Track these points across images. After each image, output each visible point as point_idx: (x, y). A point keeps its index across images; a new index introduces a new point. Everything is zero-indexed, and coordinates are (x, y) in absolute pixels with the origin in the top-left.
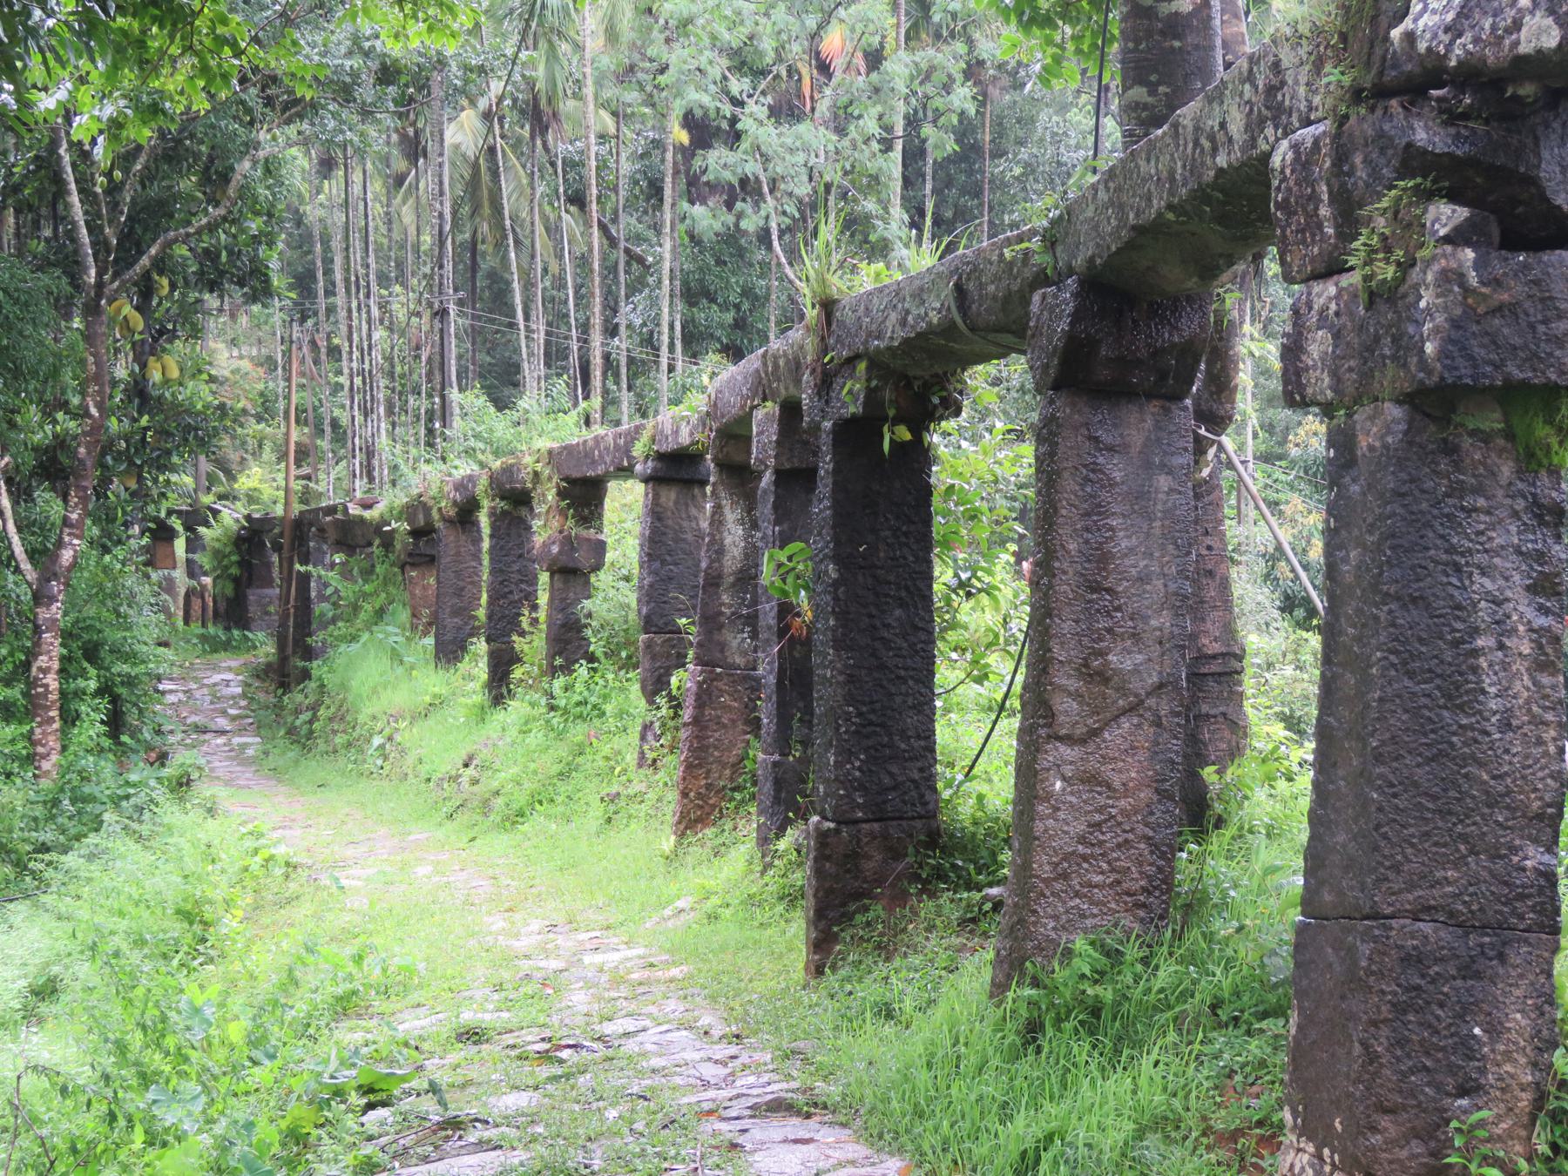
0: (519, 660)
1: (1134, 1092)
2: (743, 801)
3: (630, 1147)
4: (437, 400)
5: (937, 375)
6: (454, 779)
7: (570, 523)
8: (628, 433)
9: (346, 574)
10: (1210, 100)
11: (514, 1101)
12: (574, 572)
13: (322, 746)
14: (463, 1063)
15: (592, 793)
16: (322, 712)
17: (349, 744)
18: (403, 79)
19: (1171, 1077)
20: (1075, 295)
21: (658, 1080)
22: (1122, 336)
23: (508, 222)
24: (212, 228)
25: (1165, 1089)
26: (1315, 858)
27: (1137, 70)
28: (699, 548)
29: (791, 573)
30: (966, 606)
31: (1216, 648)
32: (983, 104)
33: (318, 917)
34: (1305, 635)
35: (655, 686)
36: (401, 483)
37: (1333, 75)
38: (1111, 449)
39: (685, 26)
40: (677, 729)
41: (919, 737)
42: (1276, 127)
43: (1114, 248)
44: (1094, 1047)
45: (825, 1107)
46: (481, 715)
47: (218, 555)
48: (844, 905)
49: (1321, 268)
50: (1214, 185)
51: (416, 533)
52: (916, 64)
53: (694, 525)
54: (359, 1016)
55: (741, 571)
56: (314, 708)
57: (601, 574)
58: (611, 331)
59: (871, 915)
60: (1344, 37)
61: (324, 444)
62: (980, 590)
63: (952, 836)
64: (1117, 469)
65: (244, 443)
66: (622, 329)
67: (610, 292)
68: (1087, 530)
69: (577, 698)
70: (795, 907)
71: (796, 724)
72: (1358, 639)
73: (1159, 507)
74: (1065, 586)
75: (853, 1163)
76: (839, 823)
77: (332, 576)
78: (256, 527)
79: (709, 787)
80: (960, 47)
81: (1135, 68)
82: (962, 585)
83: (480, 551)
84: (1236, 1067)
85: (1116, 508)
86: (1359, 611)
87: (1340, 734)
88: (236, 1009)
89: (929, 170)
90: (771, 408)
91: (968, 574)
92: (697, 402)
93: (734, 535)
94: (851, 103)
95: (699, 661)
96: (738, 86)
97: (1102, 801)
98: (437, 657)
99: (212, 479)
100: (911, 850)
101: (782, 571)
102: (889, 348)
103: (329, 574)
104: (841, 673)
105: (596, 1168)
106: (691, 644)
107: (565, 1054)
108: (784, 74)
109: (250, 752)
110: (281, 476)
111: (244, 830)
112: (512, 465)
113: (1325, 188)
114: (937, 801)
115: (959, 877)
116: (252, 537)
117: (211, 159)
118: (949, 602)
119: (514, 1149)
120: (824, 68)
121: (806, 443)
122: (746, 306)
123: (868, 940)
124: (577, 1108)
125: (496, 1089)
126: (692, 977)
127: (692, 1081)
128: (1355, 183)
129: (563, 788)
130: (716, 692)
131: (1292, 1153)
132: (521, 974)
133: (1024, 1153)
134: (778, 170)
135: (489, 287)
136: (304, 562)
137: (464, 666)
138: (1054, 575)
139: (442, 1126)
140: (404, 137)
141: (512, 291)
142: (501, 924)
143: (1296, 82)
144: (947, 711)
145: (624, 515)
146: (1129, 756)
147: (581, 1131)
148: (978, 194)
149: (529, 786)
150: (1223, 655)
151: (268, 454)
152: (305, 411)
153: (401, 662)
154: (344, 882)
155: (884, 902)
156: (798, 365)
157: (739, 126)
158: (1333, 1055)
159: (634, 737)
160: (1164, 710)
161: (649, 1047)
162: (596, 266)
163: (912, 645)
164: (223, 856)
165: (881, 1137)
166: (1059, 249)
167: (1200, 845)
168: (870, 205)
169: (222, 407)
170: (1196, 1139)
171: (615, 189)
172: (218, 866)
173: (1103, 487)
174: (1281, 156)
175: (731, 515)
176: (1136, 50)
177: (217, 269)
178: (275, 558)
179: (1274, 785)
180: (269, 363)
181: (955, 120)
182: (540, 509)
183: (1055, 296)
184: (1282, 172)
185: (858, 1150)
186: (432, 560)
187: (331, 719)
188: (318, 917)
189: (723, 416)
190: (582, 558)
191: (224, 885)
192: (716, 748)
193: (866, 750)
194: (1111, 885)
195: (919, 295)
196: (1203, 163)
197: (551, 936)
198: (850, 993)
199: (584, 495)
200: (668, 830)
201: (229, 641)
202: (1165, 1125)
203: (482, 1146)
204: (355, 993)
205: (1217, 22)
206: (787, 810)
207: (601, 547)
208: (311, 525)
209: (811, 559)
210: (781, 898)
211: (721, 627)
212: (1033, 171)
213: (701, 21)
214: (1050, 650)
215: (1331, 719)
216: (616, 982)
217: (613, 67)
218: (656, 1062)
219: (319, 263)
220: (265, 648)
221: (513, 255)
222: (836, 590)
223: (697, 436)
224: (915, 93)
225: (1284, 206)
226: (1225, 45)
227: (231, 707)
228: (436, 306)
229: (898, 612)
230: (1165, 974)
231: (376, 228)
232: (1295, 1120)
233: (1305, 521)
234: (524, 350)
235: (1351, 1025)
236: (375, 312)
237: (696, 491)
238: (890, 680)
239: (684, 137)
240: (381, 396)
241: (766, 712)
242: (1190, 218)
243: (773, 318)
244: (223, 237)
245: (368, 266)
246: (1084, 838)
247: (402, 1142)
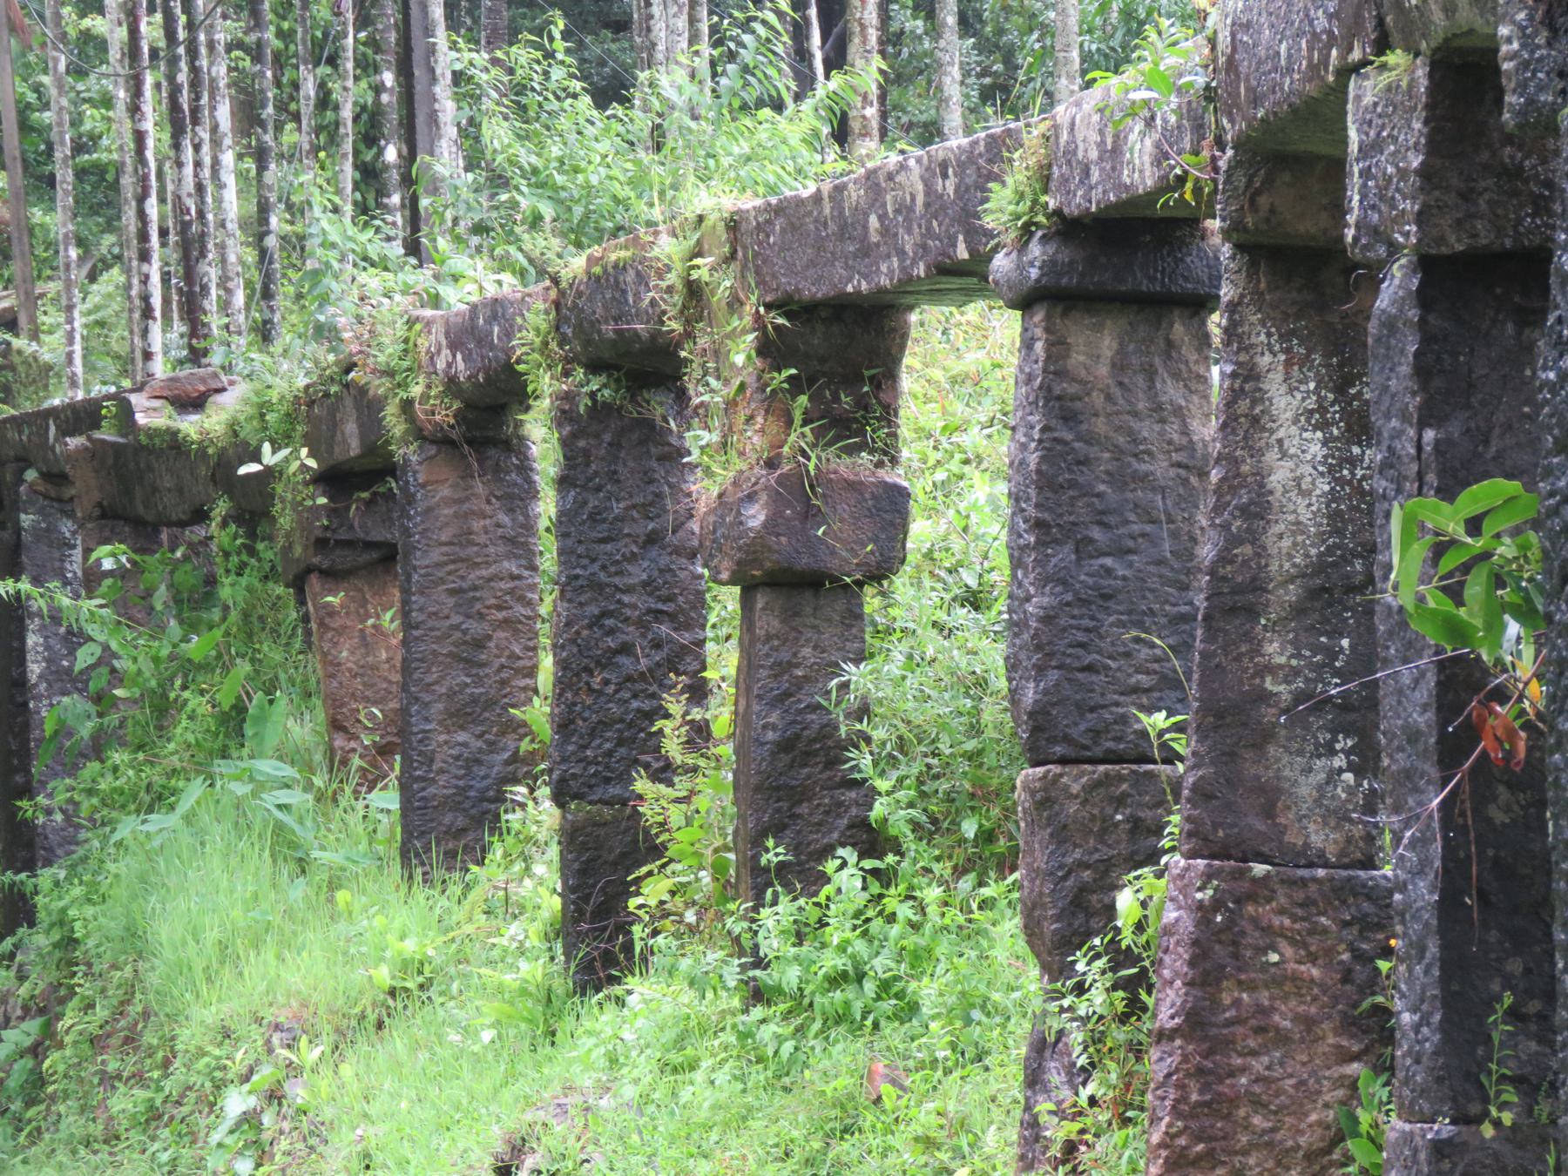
8: (968, 159)
9: (133, 607)
12: (814, 583)
13: (72, 1123)
16: (70, 1018)
17: (153, 1116)
28: (1189, 501)
35: (1069, 922)
55: (1320, 567)
56: (47, 1008)
61: (54, 220)
69: (831, 962)
83: (529, 527)
93: (1297, 461)
95: (1200, 842)
101: (1449, 562)
121: (1514, 173)
130: (1253, 937)
137: (490, 874)
153: (303, 866)
159: (1007, 1077)
175: (1287, 401)
182: (708, 393)
186: (386, 559)
187: (97, 1042)
189: (1256, 101)
190: (838, 540)
192: (1258, 1104)
199: (839, 351)
207: (891, 508)
209: (1536, 524)
211: (1266, 736)
223: (1180, 163)
241: (1408, 993)
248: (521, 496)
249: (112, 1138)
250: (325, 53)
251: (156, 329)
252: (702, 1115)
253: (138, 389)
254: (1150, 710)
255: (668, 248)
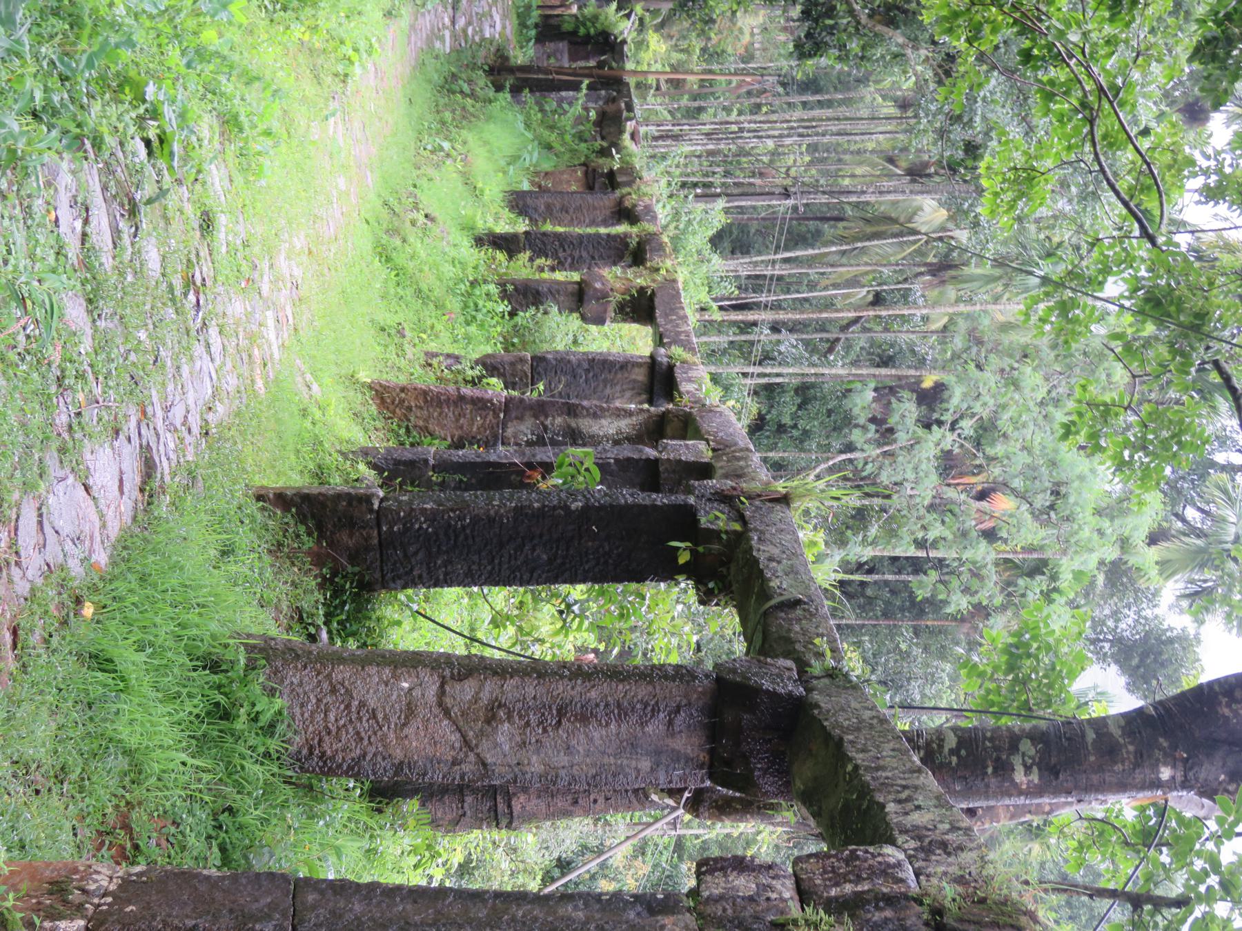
0: (511, 257)
1: (161, 747)
2: (398, 435)
3: (116, 351)
4: (718, 190)
5: (731, 586)
6: (416, 207)
7: (619, 297)
8: (689, 342)
9: (579, 120)
10: (938, 798)
11: (153, 258)
12: (579, 299)
13: (442, 101)
14: (184, 217)
15: (405, 316)
16: (469, 101)
17: (443, 123)
18: (970, 163)
19: (173, 776)
20: (790, 694)
21: (170, 370)
22: (756, 734)
23: (859, 245)
24: (851, 12)
25: (164, 771)
26: (342, 888)
27: (968, 740)
28: (600, 399)
29: (576, 474)
30: (554, 611)
31: (517, 808)
32: (955, 619)
33: (304, 100)
34: (539, 877)
35: (491, 366)
36: (653, 162)
37: (950, 891)
38: (671, 723)
39: (1013, 384)
40: (456, 383)
41: (446, 574)
42: (915, 849)
43: (826, 723)
44: (198, 716)
45: (149, 504)
46: (467, 227)
47: (595, 18)
48: (313, 517)
49: (805, 886)
50: (873, 802)
51: (611, 174)
52: (985, 566)
53: (618, 395)
54: (222, 134)
55: (580, 432)
56: (473, 95)
57: (578, 323)
58: (775, 328)
59: (305, 538)
60: (983, 901)
61: (685, 101)
62: (564, 621)
63: (368, 601)
64: (655, 728)
65: (684, 38)
66: (775, 337)
67: (805, 326)
68: (607, 705)
69: (481, 303)
70: (313, 477)
71: (457, 477)
72: (513, 919)
73: (625, 762)
74: (563, 689)
75: (104, 526)
76: (378, 512)
77: (578, 109)
78: (617, 48)
79: (409, 409)
80: (998, 600)
81: (970, 738)
82: (569, 606)
83: (598, 225)
84: (181, 827)
85: (624, 727)
86: (535, 919)
87: (439, 906)
88: (228, 35)
89: (903, 577)
90: (707, 455)
91: (577, 612)
92: (712, 395)
93: (608, 427)
94: (954, 515)
95: (509, 401)
96: (967, 426)
97: (394, 720)
98: (513, 193)
99: (655, 13)
100: (357, 569)
101: (578, 465)
102: (751, 548)
103: (579, 106)
104: (496, 513)
105: (98, 323)
106: (523, 393)
107: (192, 297)
108: (978, 462)
109: (438, 45)
110: (659, 67)
111: (373, 40)
112: (664, 251)
113: (866, 888)
114: (396, 589)
115: (336, 607)
116: (608, 45)
117: (905, 12)
118: (557, 596)
119: (114, 258)
120: (982, 496)
121: (679, 484)
122: (795, 433)
123: (285, 536)
124: (148, 307)
125: (163, 242)
126: (256, 397)
127: (170, 398)
128: (869, 911)
129: (409, 292)
130: (484, 413)
131: (108, 873)
132: (257, 262)
133: (110, 661)
134: (900, 458)
135: (809, 231)
136: (590, 87)
137: (507, 214)
138: (570, 680)
139: (132, 201)
140: (926, 165)
141: (806, 249)
142: (298, 246)
143: (950, 865)
144: (470, 595)
145: (626, 339)
146: (429, 742)
147: (128, 311)
148: (886, 615)
149: (411, 265)
150: (511, 813)
151: (676, 57)
152: (711, 86)
153: (509, 164)
154: (332, 120)
155: (316, 549)
156: (739, 476)
157: (935, 427)
158: (185, 904)
159: (449, 349)
160: (466, 768)
161: (198, 364)
162: (825, 315)
163: (518, 568)
164: (352, 24)
165: (125, 548)
166: (826, 681)
167: (360, 796)
168: (873, 531)
169: (713, 21)
170: (123, 796)
171: (886, 330)
172: (343, 20)
173: (641, 718)
174: (891, 853)
175: (624, 425)
176: (985, 738)
177: (819, 17)
178: (592, 63)
179: (409, 854)
180: (748, 57)
181: (941, 597)
182: (630, 273)
183: (789, 678)
184: (880, 855)
185: (114, 530)
186: (590, 187)
187: (464, 108)
188: (304, 100)
189: (701, 417)
190: (591, 306)
191: (328, 25)
192: (440, 414)
193: (436, 533)
194: (327, 727)
195: (792, 571)
196: (889, 792)
197: (289, 285)
198: (242, 522)
199: (641, 308)
200: (376, 376)
201: (526, 27)
202: (136, 772)
203: (116, 232)
204: (241, 130)
205: (1007, 802)
206: (389, 471)
207: (600, 321)
208: (619, 92)
209: (586, 488)
210: (319, 467)
211: (536, 417)
212: (903, 659)
213: (1017, 397)
214: (512, 677)
215: (451, 898)
216: (251, 337)
217: (981, 328)
218: (185, 370)
219: (826, 97)
220: (521, 56)
221: (834, 249)
222: (561, 508)
223: (686, 398)
224: (962, 565)
225: (854, 856)
226: (990, 808)
227: (474, 29)
228: (793, 189)
229: (545, 557)
230: (256, 770)
231: (856, 142)
232: (136, 875)
233: (629, 877)
234: (759, 258)
235: (209, 918)
236: (788, 141)
237: (644, 397)
238: (491, 551)
239: (928, 383)
240: (722, 146)
241: (469, 453)
242: (848, 783)
243: (786, 454)
244: (845, 21)
245: (824, 135)
246: (364, 706)
247: (119, 170)
248: (605, 223)
249: (438, 112)
250: (727, 174)
251: (654, 128)
252: (441, 269)
253: (637, 122)
254: (545, 386)
255: (669, 263)
